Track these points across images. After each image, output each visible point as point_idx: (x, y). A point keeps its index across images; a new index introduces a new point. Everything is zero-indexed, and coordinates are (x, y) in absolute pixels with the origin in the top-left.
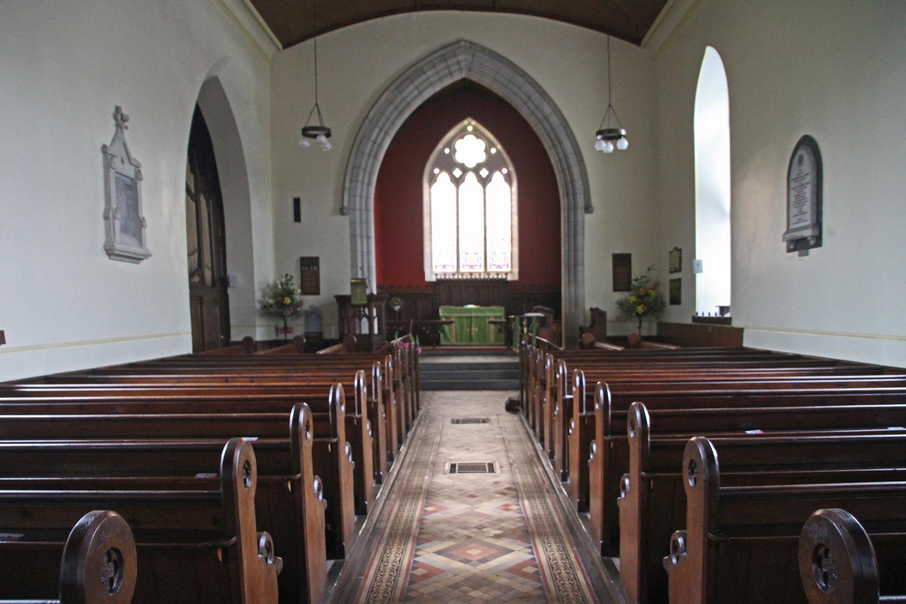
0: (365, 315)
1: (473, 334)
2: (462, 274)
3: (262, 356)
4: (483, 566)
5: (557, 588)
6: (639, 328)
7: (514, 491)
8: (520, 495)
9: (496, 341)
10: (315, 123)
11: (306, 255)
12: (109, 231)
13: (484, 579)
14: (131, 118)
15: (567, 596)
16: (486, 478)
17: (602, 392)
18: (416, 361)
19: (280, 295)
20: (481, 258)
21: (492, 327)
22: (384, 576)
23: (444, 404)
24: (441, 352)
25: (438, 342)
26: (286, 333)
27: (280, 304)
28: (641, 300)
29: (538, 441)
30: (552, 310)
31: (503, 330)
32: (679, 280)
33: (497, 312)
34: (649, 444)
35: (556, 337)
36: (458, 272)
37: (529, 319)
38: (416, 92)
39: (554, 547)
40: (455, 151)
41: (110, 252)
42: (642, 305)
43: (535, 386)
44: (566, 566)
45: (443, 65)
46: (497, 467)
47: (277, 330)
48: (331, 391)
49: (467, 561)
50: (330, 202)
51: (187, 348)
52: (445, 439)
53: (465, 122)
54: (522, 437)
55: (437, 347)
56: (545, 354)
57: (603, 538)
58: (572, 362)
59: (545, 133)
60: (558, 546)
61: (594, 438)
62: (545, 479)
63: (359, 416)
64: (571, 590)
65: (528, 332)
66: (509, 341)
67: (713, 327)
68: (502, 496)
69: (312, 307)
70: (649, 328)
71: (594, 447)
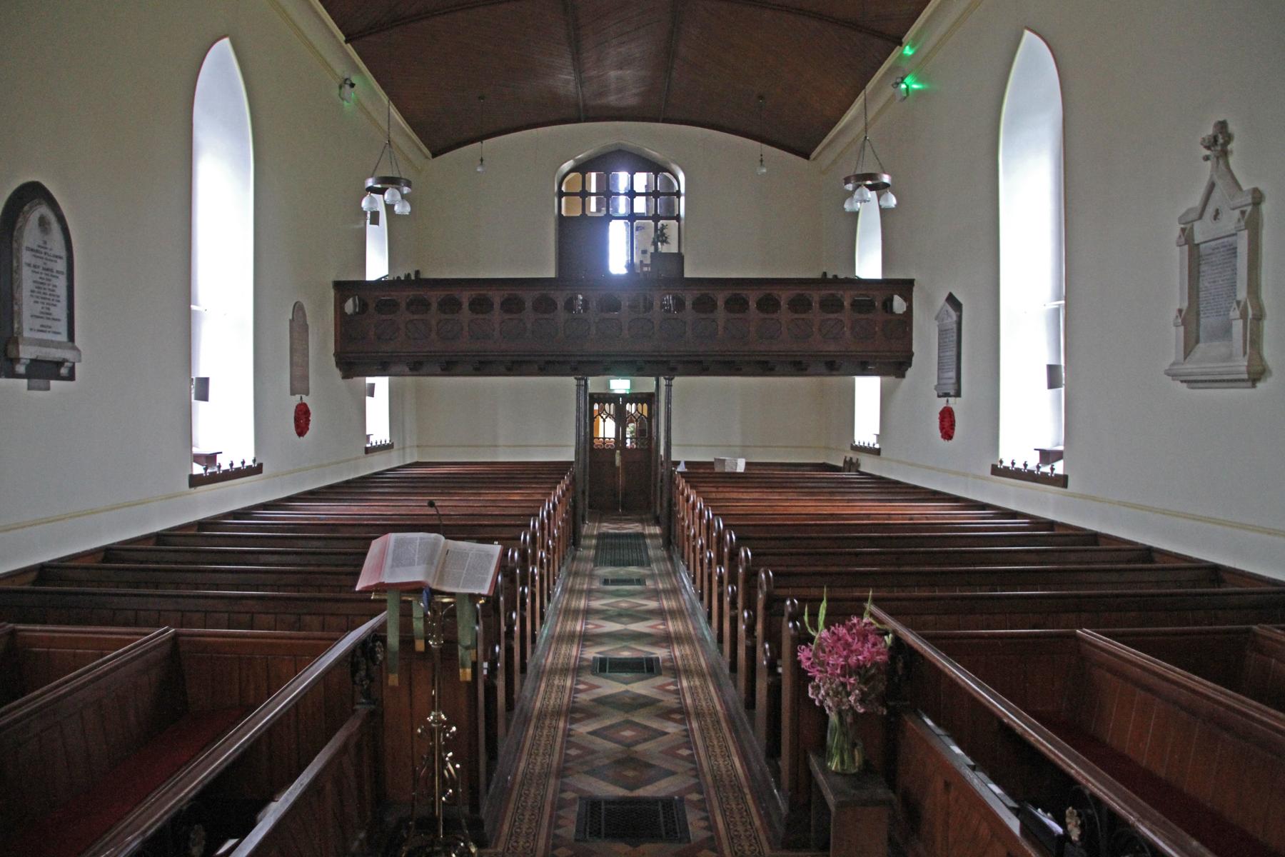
22: (527, 827)
39: (680, 624)
51: (635, 211)
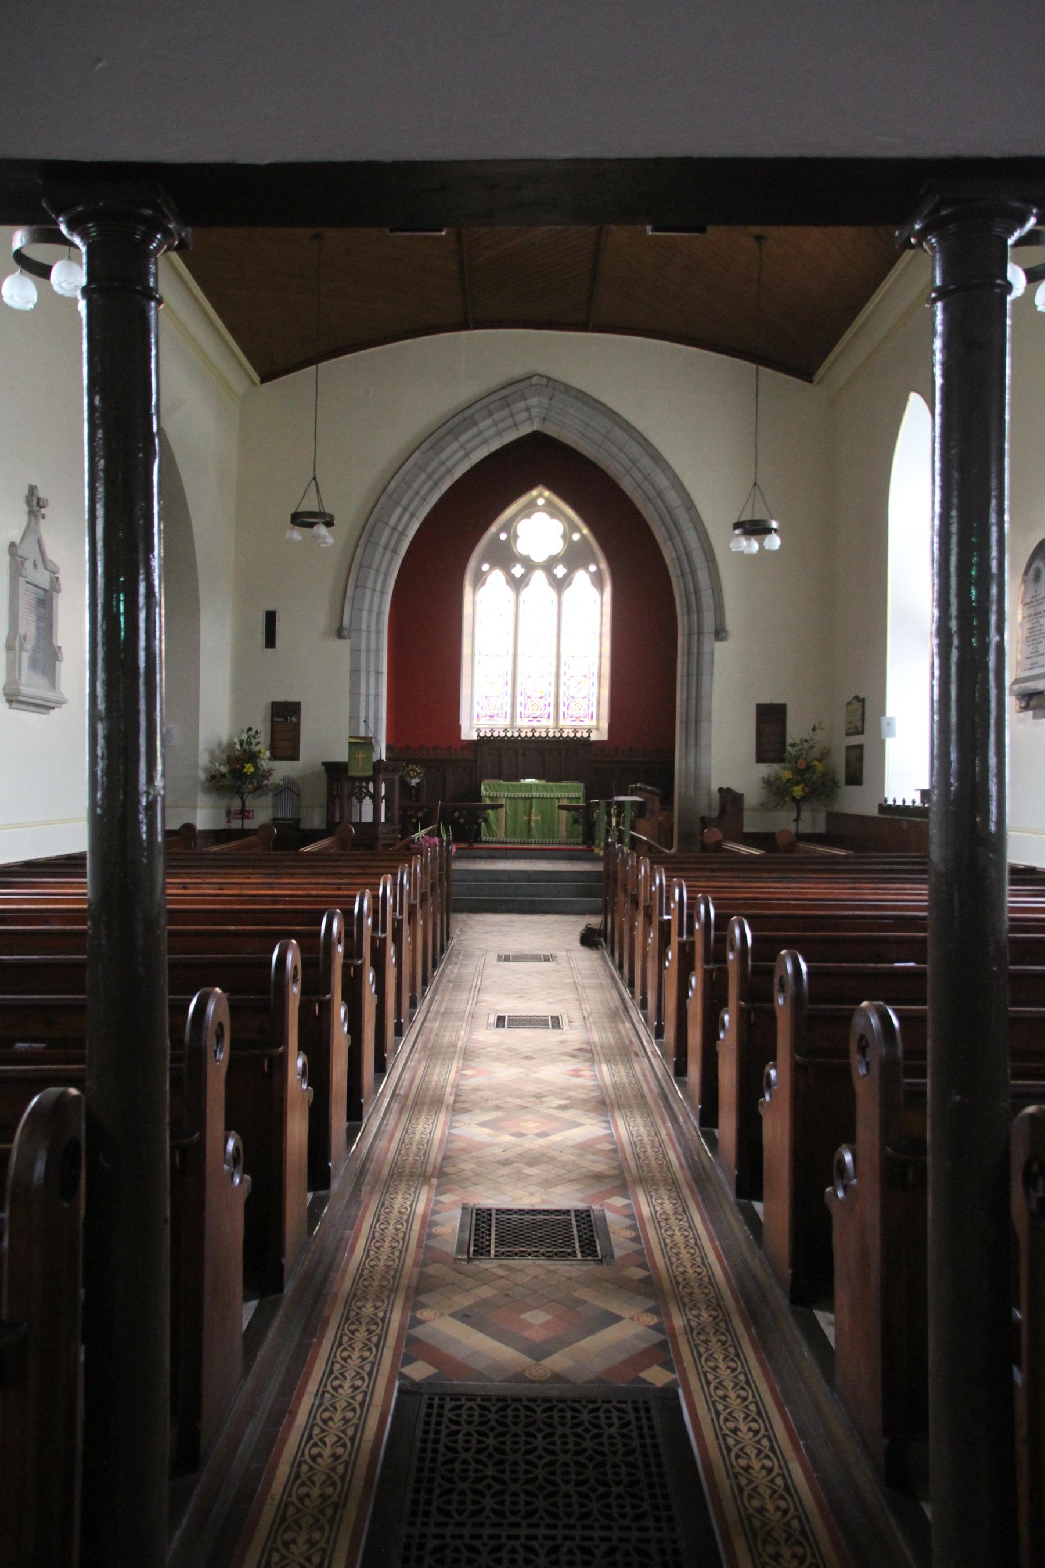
0: (368, 792)
1: (533, 825)
2: (520, 731)
3: (215, 854)
4: (543, 1141)
5: (667, 1260)
6: (797, 820)
7: (588, 1053)
8: (596, 1057)
9: (569, 837)
10: (310, 505)
11: (281, 698)
12: (13, 667)
13: (544, 1155)
14: (51, 502)
15: (691, 1294)
16: (548, 1037)
17: (702, 908)
18: (448, 866)
19: (237, 759)
20: (549, 705)
21: (564, 813)
23: (486, 933)
24: (484, 853)
25: (477, 837)
26: (242, 819)
27: (237, 773)
28: (799, 778)
29: (626, 986)
30: (658, 791)
31: (581, 820)
32: (860, 747)
33: (571, 791)
34: (750, 968)
35: (665, 835)
36: (513, 727)
37: (621, 804)
38: (461, 453)
39: (640, 1121)
40: (516, 537)
41: (13, 699)
42: (802, 786)
43: (625, 902)
44: (701, 1279)
45: (505, 412)
46: (564, 1021)
47: (229, 813)
48: (358, 899)
49: (520, 1135)
50: (322, 618)
52: (487, 982)
53: (534, 493)
54: (604, 982)
55: (476, 846)
56: (638, 857)
57: (702, 1102)
58: (675, 868)
59: (657, 518)
60: (674, 1204)
61: (693, 969)
62: (635, 1039)
63: (383, 936)
64: (684, 1245)
65: (618, 824)
66: (589, 837)
67: (909, 821)
68: (569, 1058)
69: (285, 779)
70: (813, 822)
71: (726, 1018)
